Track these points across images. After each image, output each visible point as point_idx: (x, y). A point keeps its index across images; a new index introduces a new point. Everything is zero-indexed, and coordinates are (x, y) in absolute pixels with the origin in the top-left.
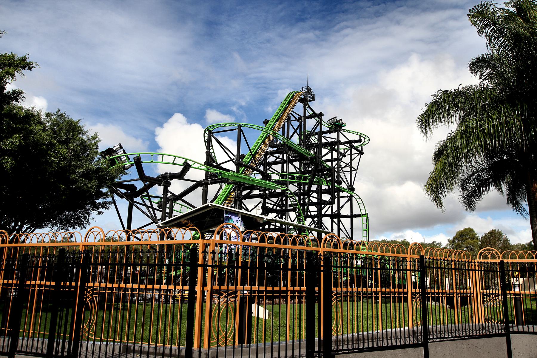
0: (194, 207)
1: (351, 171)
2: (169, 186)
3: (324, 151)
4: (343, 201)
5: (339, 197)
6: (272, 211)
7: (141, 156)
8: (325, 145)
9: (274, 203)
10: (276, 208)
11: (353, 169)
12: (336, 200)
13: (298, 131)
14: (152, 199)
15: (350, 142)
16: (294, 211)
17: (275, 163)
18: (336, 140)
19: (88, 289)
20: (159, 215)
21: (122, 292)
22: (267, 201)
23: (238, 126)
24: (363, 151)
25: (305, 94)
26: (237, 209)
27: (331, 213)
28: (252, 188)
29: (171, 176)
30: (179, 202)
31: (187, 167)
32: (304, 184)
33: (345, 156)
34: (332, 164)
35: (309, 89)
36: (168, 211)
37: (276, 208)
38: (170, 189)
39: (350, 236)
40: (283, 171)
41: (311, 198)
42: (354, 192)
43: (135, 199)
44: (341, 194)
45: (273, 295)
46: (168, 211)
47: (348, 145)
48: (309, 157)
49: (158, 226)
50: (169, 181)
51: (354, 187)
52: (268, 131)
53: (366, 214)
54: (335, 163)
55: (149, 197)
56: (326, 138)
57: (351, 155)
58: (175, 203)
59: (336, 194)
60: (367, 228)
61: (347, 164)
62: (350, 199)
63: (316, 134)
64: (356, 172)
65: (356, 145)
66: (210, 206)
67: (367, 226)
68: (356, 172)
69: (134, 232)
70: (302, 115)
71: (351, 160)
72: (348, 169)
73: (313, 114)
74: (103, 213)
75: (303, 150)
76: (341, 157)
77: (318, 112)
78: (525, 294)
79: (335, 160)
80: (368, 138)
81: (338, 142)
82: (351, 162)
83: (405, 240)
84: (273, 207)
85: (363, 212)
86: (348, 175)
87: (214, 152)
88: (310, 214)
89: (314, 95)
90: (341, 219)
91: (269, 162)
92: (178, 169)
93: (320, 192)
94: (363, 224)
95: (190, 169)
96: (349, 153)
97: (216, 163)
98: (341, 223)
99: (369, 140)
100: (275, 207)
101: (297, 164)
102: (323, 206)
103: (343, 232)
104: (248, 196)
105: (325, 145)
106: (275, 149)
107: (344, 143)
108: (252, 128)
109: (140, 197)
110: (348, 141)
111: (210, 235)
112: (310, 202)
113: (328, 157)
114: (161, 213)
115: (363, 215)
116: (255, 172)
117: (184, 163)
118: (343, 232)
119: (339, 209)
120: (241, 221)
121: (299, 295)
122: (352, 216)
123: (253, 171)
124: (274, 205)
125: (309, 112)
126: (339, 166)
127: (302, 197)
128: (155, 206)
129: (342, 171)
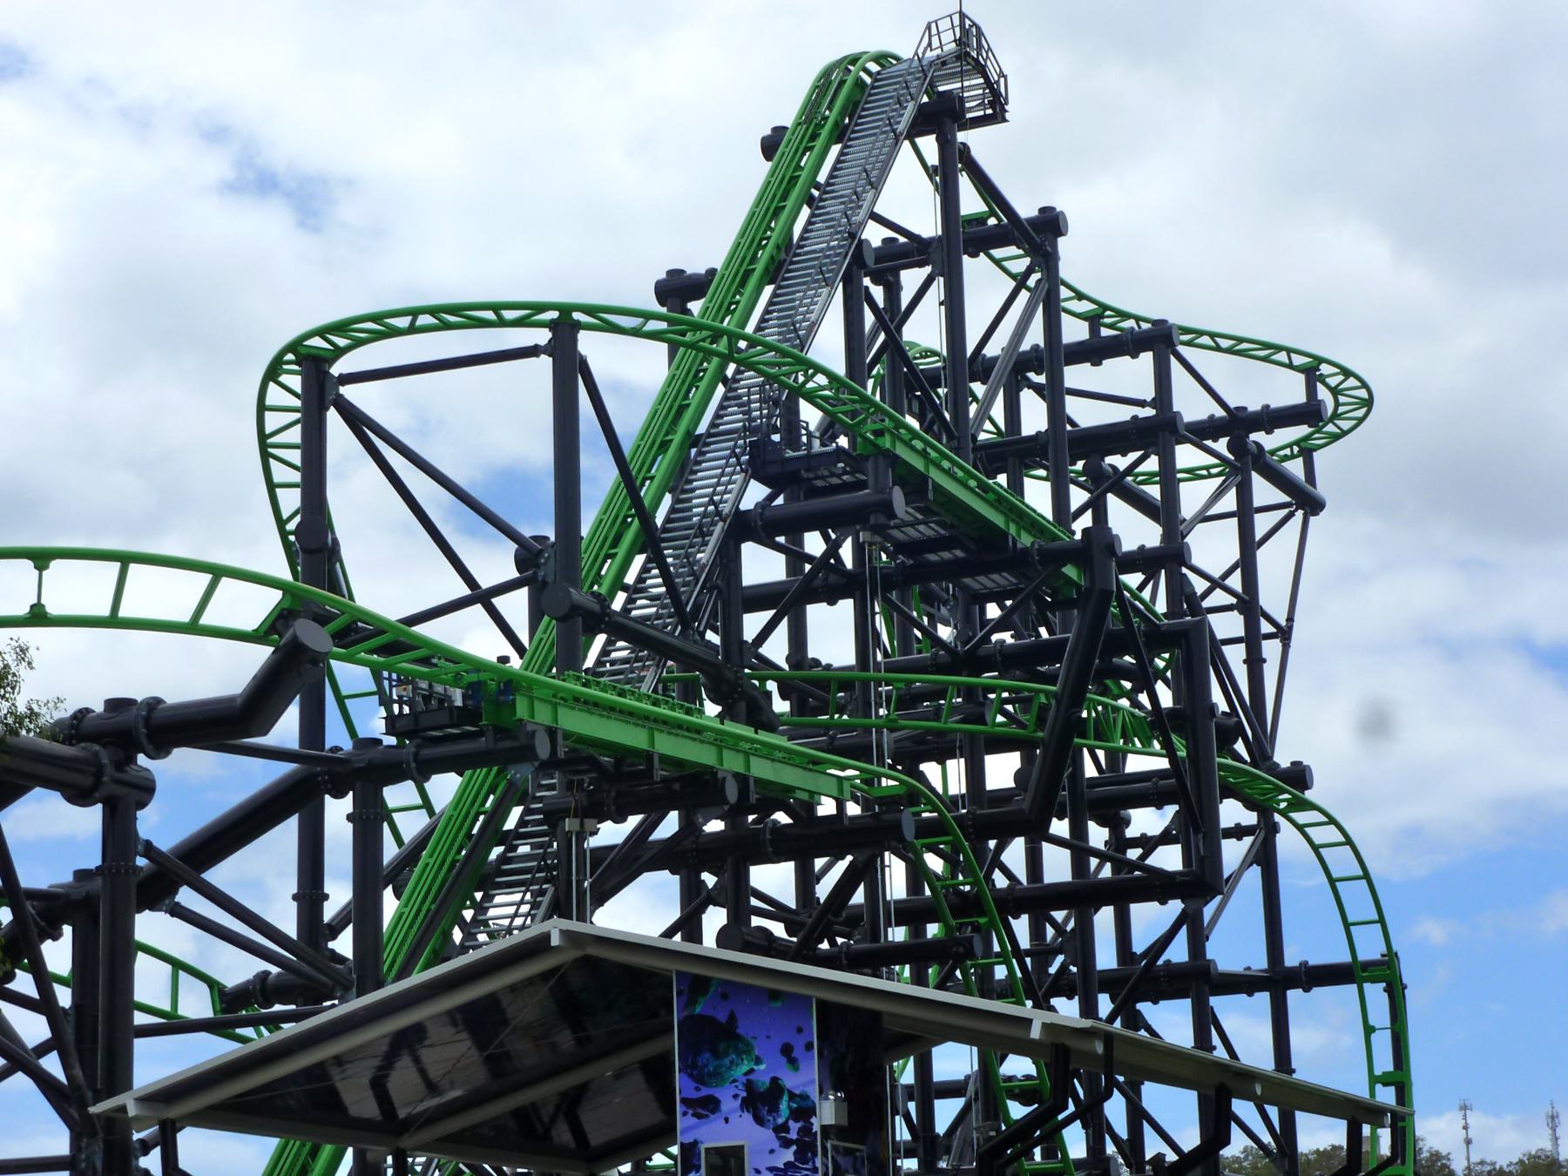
1: (1252, 640)
11: (1266, 627)
18: (1149, 412)
24: (1323, 489)
42: (1309, 795)
47: (1221, 446)
53: (1386, 971)
56: (1345, 392)
57: (1245, 513)
71: (1249, 545)
82: (1247, 563)
85: (1370, 947)
89: (1002, 75)
90: (1216, 1002)
94: (1369, 1030)
107: (1201, 433)
110: (1220, 413)
115: (1367, 965)
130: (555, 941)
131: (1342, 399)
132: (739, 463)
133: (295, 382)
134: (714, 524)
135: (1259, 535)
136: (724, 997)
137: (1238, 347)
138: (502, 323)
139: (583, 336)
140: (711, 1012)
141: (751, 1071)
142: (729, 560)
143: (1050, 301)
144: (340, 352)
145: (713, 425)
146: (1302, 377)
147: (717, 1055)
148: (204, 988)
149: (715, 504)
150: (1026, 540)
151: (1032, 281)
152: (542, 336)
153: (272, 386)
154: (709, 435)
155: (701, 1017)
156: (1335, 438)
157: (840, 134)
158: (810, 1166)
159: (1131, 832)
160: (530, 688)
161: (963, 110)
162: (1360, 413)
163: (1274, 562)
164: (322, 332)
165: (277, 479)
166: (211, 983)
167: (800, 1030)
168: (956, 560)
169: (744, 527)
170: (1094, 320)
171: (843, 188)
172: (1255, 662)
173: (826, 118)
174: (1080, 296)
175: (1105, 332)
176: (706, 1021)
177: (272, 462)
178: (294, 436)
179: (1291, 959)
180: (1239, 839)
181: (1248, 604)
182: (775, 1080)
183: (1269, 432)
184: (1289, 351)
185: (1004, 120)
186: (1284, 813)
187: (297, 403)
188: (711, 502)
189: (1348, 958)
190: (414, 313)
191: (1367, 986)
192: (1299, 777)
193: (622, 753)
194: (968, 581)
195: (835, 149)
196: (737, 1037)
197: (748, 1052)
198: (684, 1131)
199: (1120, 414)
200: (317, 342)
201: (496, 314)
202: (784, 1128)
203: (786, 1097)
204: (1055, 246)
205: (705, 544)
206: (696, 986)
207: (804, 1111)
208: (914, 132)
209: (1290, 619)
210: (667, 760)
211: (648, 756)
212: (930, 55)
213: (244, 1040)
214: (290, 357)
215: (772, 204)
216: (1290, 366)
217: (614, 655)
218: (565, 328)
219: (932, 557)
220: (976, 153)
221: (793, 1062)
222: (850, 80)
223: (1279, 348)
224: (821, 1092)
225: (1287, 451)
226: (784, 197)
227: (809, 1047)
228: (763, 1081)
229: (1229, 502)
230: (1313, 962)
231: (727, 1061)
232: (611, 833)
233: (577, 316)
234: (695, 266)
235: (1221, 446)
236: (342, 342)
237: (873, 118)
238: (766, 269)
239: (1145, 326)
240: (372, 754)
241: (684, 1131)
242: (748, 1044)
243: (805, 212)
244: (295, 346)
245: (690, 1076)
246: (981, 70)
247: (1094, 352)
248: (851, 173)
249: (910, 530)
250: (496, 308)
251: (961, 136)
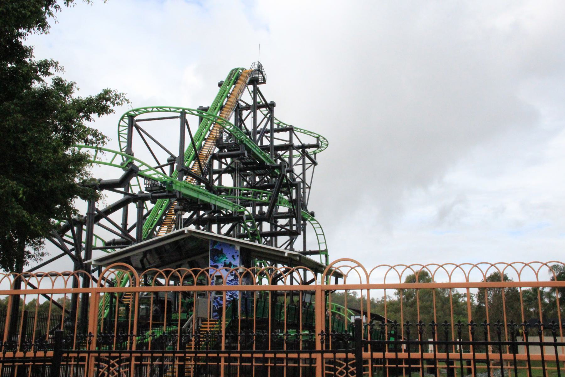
11: (306, 186)
15: (303, 147)
18: (288, 143)
19: (111, 361)
21: (269, 364)
26: (237, 238)
35: (260, 66)
39: (303, 280)
42: (314, 218)
45: (397, 366)
47: (300, 150)
57: (304, 164)
66: (186, 233)
71: (304, 170)
78: (529, 360)
80: (327, 143)
82: (304, 173)
85: (323, 248)
89: (265, 75)
107: (298, 148)
115: (322, 251)
121: (408, 366)
130: (186, 232)
131: (323, 144)
132: (214, 144)
133: (127, 121)
134: (209, 155)
135: (306, 168)
137: (305, 132)
138: (171, 111)
139: (187, 115)
140: (218, 248)
141: (225, 260)
142: (211, 164)
143: (271, 119)
144: (137, 115)
145: (209, 136)
146: (316, 139)
147: (218, 257)
148: (101, 241)
149: (209, 152)
150: (268, 164)
151: (268, 116)
152: (179, 114)
153: (122, 121)
154: (208, 138)
156: (321, 151)
157: (235, 83)
158: (237, 280)
159: (279, 224)
160: (176, 183)
161: (258, 81)
162: (326, 147)
163: (308, 173)
164: (133, 111)
165: (121, 140)
166: (103, 241)
167: (236, 252)
169: (214, 157)
170: (278, 125)
171: (235, 94)
172: (304, 192)
173: (232, 79)
174: (276, 119)
175: (280, 127)
176: (216, 250)
177: (120, 137)
178: (126, 132)
179: (308, 249)
181: (304, 181)
182: (230, 263)
183: (309, 149)
184: (314, 133)
185: (265, 83)
186: (309, 221)
187: (127, 125)
188: (209, 151)
189: (319, 250)
190: (153, 108)
191: (322, 255)
192: (313, 214)
193: (192, 198)
194: (256, 171)
195: (233, 86)
196: (223, 254)
197: (225, 257)
199: (282, 143)
200: (132, 113)
201: (170, 110)
202: (232, 272)
203: (232, 266)
204: (273, 109)
205: (207, 159)
206: (214, 243)
208: (246, 85)
209: (311, 185)
210: (201, 200)
211: (198, 199)
212: (253, 69)
213: (109, 252)
214: (126, 115)
215: (220, 97)
216: (314, 136)
217: (188, 180)
218: (183, 113)
219: (249, 166)
220: (260, 89)
221: (234, 259)
222: (237, 72)
223: (312, 133)
224: (240, 265)
225: (311, 153)
226: (224, 93)
227: (238, 256)
228: (228, 262)
229: (301, 162)
230: (311, 250)
231: (220, 258)
232: (187, 215)
233: (186, 111)
234: (205, 106)
235: (300, 150)
236: (137, 113)
237: (241, 80)
238: (220, 107)
239: (287, 126)
240: (143, 195)
241: (211, 272)
243: (226, 99)
244: (127, 113)
245: (212, 261)
246: (262, 73)
247: (278, 131)
248: (237, 91)
249: (246, 160)
250: (170, 108)
251: (258, 86)
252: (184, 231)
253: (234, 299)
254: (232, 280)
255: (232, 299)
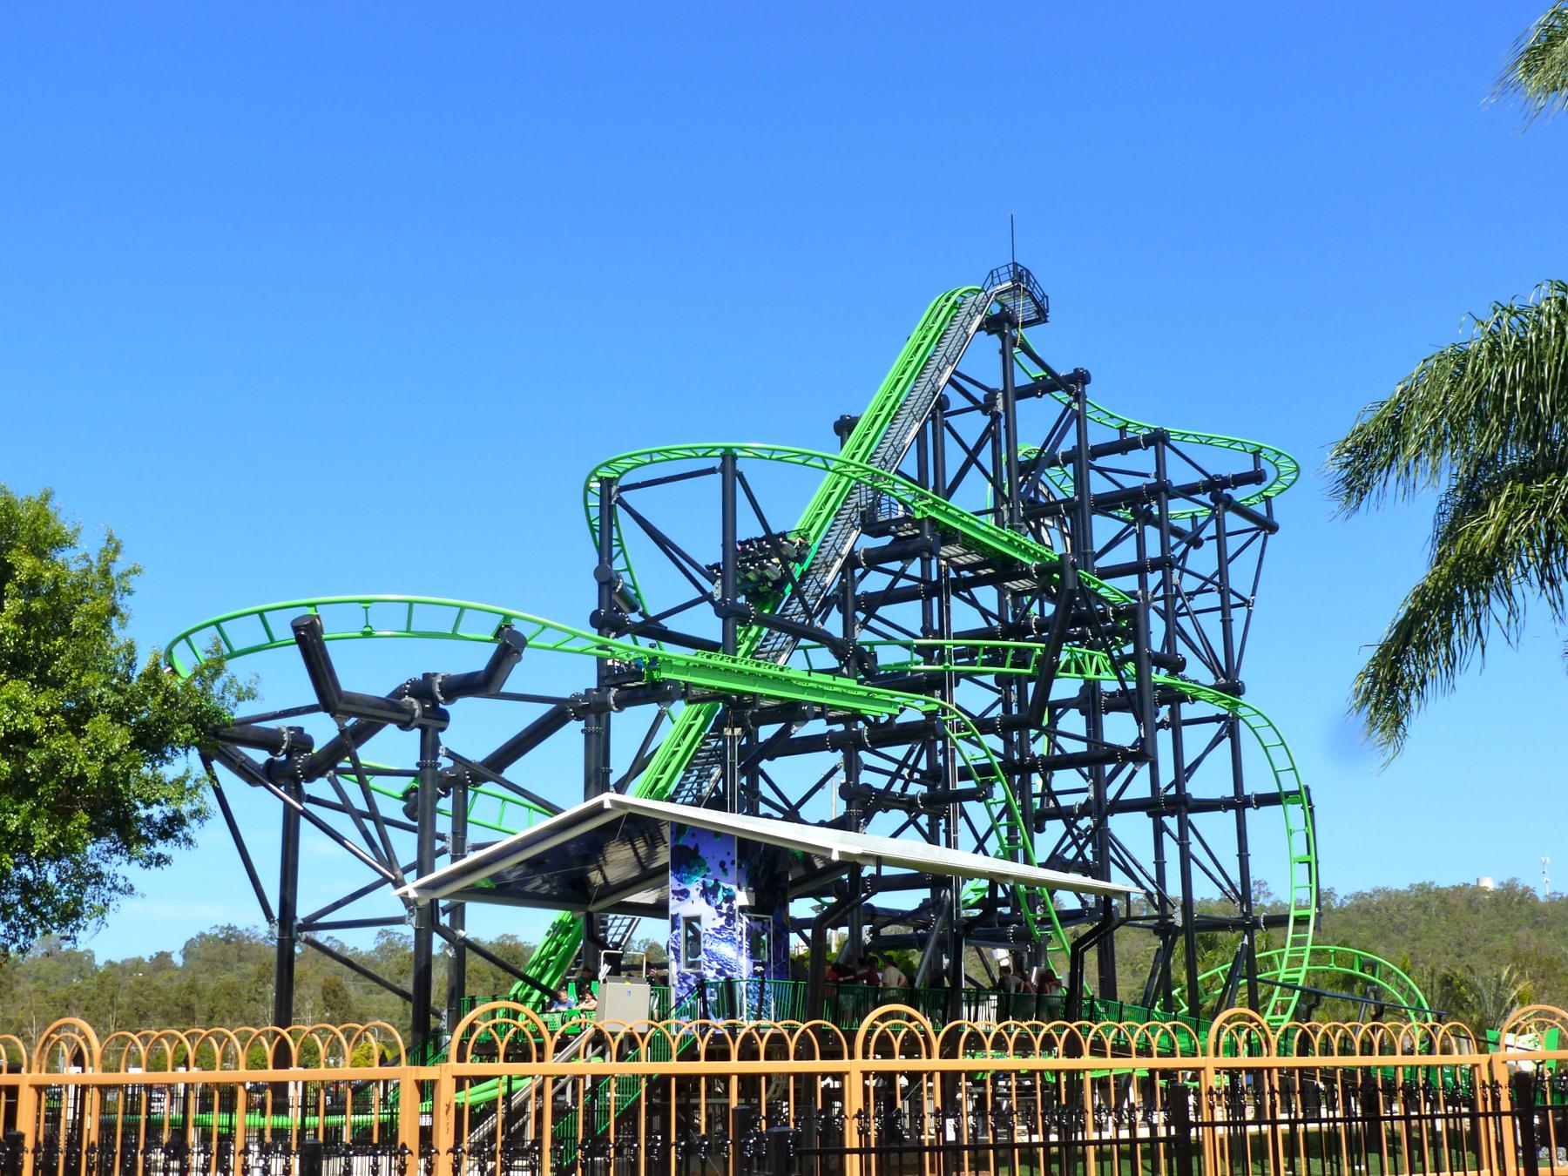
0: (555, 810)
1: (1225, 609)
2: (443, 729)
3: (1103, 528)
4: (1195, 739)
5: (1176, 724)
6: (884, 800)
7: (321, 611)
8: (1106, 504)
9: (893, 767)
10: (905, 788)
12: (1164, 738)
13: (986, 457)
14: (374, 782)
16: (979, 800)
17: (892, 596)
18: (1153, 480)
20: (405, 846)
22: (866, 757)
23: (723, 456)
24: (1277, 518)
25: (1006, 296)
27: (1149, 795)
28: (791, 712)
29: (105, 1125)
30: (488, 787)
31: (509, 646)
32: (1021, 681)
33: (1196, 542)
34: (1143, 584)
36: (444, 825)
37: (905, 788)
38: (447, 739)
40: (927, 631)
41: (1059, 739)
43: (309, 788)
44: (1187, 711)
46: (444, 825)
48: (1033, 564)
49: (405, 899)
50: (441, 706)
51: (1241, 678)
52: (852, 468)
53: (1302, 796)
54: (1154, 578)
55: (361, 773)
57: (1221, 537)
58: (476, 793)
59: (1164, 712)
60: (1309, 853)
61: (1207, 581)
62: (1230, 727)
63: (1068, 458)
64: (1250, 612)
65: (1240, 494)
66: (608, 810)
67: (1311, 843)
68: (1250, 612)
69: (311, 924)
70: (996, 382)
71: (1224, 561)
72: (1214, 599)
73: (1044, 377)
74: (167, 861)
75: (1006, 539)
76: (1178, 552)
77: (1063, 371)
79: (1156, 565)
81: (1162, 490)
82: (1222, 571)
83: (1514, 880)
84: (891, 784)
85: (1289, 785)
86: (1212, 625)
87: (629, 569)
88: (1056, 802)
89: (1045, 296)
90: (1192, 817)
91: (866, 594)
92: (476, 659)
93: (1092, 703)
95: (526, 652)
96: (1211, 529)
97: (642, 614)
98: (1192, 837)
99: (1298, 470)
100: (897, 787)
101: (987, 596)
102: (1109, 768)
103: (1204, 869)
104: (784, 746)
105: (1106, 504)
106: (886, 540)
107: (1188, 491)
108: (779, 459)
109: (329, 779)
110: (1206, 479)
111: (627, 922)
112: (1057, 752)
113: (1125, 553)
114: (414, 837)
115: (1288, 794)
116: (803, 642)
117: (500, 629)
118: (1204, 869)
119: (1183, 773)
120: (739, 867)
122: (1239, 803)
123: (796, 639)
124: (895, 776)
125: (1028, 371)
126: (1171, 593)
127: (1016, 737)
128: (392, 808)
129: (1184, 610)
136: (693, 835)
140: (686, 844)
155: (681, 846)
168: (989, 574)
176: (685, 848)
180: (1219, 722)
196: (699, 857)
198: (674, 907)
203: (721, 890)
207: (730, 899)
219: (982, 572)
221: (725, 871)
227: (733, 863)
241: (674, 907)
242: (703, 861)
252: (601, 804)
253: (729, 979)
254: (722, 927)
255: (722, 978)
